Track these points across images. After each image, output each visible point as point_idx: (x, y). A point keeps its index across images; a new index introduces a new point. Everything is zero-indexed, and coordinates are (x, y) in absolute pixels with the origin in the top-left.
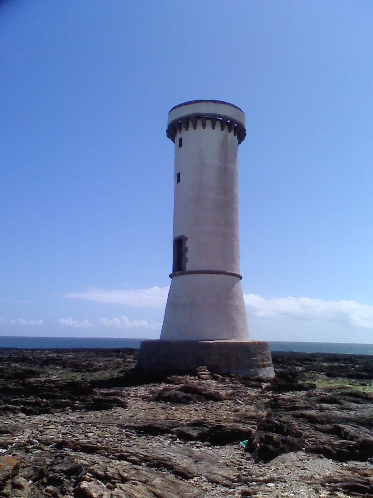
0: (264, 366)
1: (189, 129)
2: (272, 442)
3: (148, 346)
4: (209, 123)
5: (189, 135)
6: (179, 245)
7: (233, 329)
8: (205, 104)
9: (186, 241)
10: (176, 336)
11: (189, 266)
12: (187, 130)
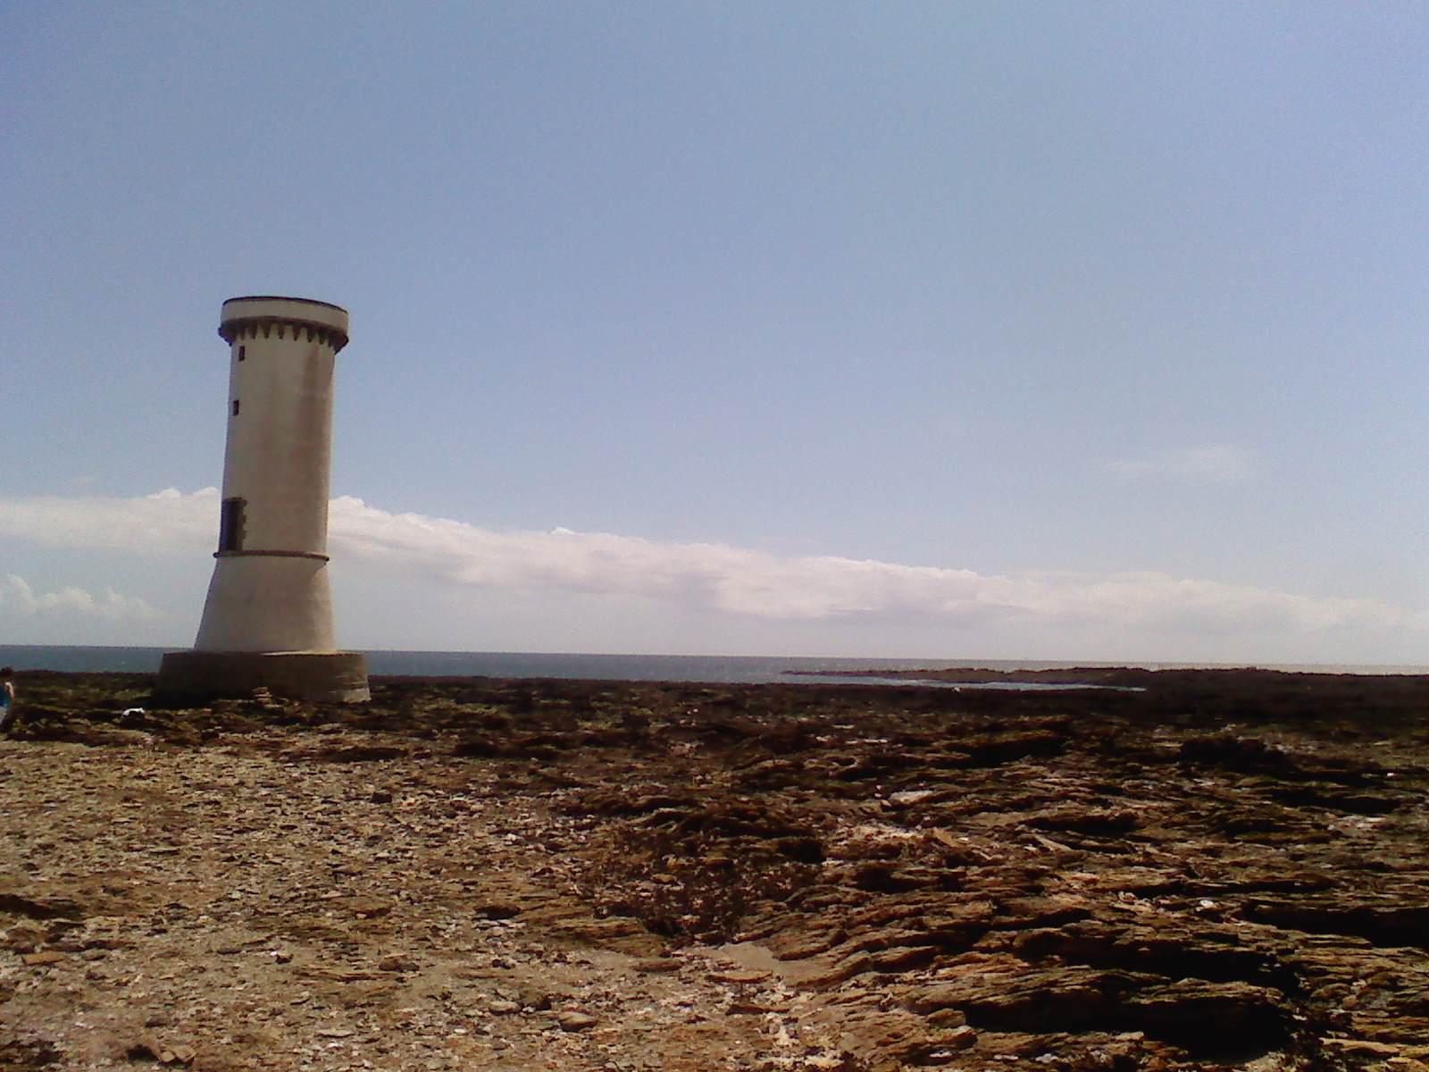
0: (353, 687)
2: (1286, 1029)
3: (176, 662)
4: (289, 330)
5: (258, 345)
6: (233, 512)
7: (310, 635)
10: (223, 645)
11: (247, 544)
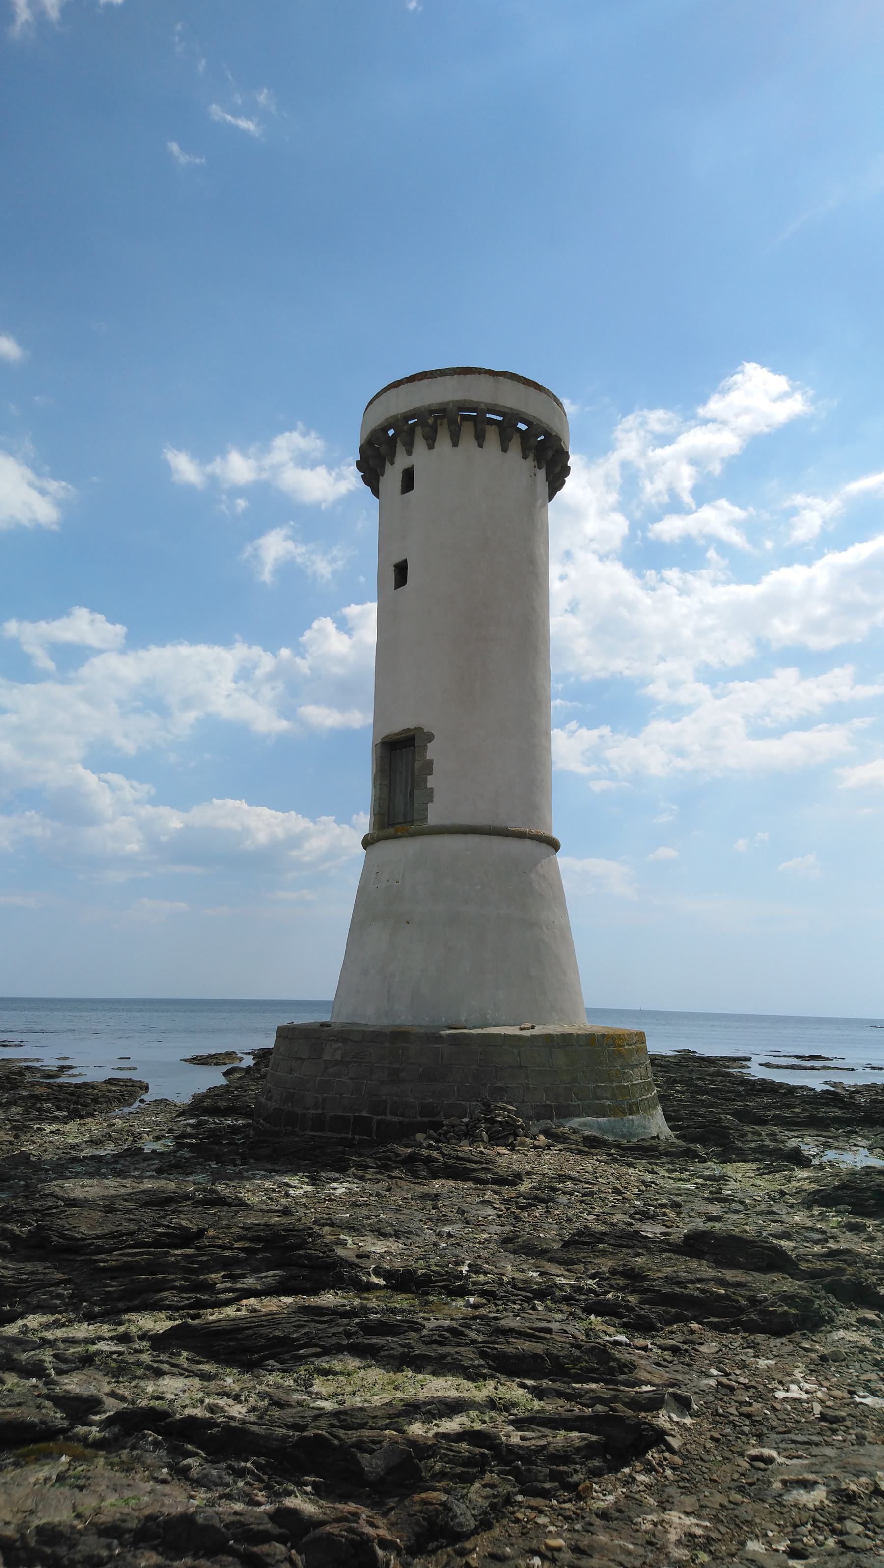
1: (436, 445)
8: (490, 379)
9: (429, 745)
12: (431, 447)
